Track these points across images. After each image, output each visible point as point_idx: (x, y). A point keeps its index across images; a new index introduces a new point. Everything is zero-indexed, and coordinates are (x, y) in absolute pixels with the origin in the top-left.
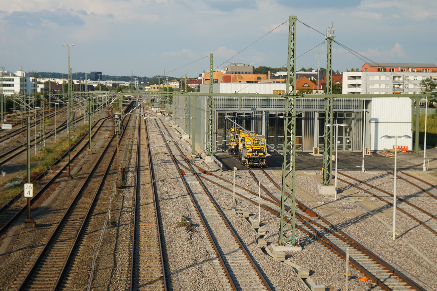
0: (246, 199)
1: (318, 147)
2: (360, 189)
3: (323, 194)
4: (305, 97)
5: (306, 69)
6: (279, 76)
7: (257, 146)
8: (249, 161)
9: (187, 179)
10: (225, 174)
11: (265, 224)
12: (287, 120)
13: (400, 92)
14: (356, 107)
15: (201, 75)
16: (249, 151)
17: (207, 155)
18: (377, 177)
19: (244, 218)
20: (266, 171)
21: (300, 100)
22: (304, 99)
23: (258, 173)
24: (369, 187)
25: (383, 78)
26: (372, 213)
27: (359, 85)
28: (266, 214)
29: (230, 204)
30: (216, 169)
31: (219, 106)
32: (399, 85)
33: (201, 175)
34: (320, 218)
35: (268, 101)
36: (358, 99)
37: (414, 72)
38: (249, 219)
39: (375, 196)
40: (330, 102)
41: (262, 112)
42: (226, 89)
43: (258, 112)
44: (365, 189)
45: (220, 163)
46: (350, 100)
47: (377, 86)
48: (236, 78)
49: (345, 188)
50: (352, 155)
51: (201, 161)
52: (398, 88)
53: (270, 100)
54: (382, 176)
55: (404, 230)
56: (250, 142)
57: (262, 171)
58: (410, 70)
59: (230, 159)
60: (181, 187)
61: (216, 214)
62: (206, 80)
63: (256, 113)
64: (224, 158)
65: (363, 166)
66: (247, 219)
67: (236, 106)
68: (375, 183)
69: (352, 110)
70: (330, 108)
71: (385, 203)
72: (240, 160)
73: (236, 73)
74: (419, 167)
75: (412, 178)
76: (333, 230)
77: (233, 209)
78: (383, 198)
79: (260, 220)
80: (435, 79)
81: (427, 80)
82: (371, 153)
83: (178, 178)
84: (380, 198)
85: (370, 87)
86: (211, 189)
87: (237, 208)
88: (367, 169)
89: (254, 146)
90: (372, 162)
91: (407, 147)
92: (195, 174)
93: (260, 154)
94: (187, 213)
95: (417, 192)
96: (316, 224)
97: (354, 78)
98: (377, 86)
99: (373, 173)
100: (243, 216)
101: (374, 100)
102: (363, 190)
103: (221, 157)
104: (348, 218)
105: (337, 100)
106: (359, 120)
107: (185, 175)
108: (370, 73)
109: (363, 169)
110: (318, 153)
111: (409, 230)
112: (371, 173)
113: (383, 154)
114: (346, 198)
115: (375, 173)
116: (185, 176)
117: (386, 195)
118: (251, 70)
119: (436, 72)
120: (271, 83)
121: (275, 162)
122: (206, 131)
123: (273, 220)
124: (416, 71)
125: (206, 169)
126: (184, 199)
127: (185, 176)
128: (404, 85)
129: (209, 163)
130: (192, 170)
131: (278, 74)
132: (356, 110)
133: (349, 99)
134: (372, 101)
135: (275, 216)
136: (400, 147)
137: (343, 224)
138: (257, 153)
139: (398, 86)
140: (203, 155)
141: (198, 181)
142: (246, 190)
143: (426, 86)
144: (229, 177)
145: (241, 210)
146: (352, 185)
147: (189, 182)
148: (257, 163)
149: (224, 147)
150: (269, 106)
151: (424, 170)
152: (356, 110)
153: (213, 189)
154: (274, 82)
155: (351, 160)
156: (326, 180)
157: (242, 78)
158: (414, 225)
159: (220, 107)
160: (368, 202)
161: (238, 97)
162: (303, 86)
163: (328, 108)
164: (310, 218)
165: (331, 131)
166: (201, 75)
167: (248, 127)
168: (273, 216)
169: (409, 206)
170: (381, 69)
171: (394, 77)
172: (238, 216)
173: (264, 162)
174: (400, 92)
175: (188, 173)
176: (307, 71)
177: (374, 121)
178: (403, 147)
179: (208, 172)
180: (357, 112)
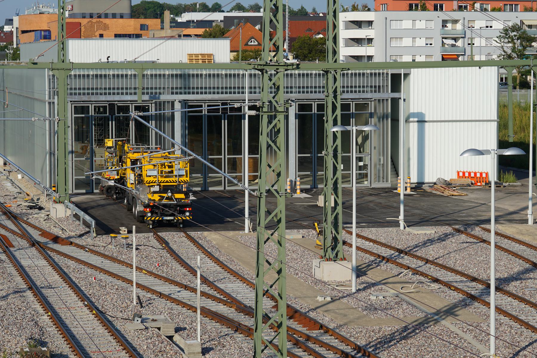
0: (161, 295)
1: (298, 179)
2: (402, 266)
3: (326, 279)
4: (304, 69)
5: (246, 5)
6: (188, 22)
7: (171, 179)
8: (152, 212)
9: (17, 254)
10: (102, 242)
11: (212, 349)
12: (265, 120)
13: (458, 56)
14: (378, 89)
15: (12, 20)
16: (152, 189)
17: (55, 202)
18: (431, 241)
19: (163, 337)
20: (192, 234)
21: (291, 75)
22: (301, 72)
23: (176, 239)
24: (421, 263)
25: (421, 25)
26: (436, 317)
27: (370, 41)
28: (209, 327)
29: (127, 307)
30: (78, 233)
31: (86, 91)
32: (455, 39)
33: (48, 245)
34: (327, 331)
35: (184, 78)
36: (381, 71)
37: (486, 10)
38: (175, 339)
39: (436, 280)
40: (335, 79)
41: (173, 103)
42: (83, 52)
43: (164, 102)
44: (413, 266)
45: (88, 218)
46: (364, 74)
47: (407, 42)
48: (92, 26)
49: (369, 266)
50: (371, 195)
51: (43, 214)
52: (453, 46)
53: (189, 75)
54: (442, 239)
55: (511, 351)
56: (160, 167)
57: (182, 234)
58: (477, 5)
59: (110, 209)
60: (10, 275)
61: (101, 330)
62: (24, 32)
63: (160, 105)
64: (93, 208)
65: (401, 217)
66: (171, 338)
67: (120, 90)
68: (431, 252)
69: (369, 95)
70: (335, 91)
71: (461, 296)
72: (130, 210)
73: (91, 16)
74: (516, 217)
75: (506, 240)
76: (359, 355)
77: (136, 318)
78: (455, 284)
79: (201, 339)
80: (530, 26)
81: (514, 28)
82: (412, 188)
83: (15, 251)
84: (448, 285)
85: (394, 43)
86: (78, 275)
87: (144, 316)
88: (409, 223)
89: (163, 179)
90: (417, 208)
91: (487, 174)
92: (34, 243)
93: (178, 196)
94: (36, 330)
95: (521, 269)
96: (323, 344)
97: (358, 24)
98: (407, 42)
99: (423, 232)
100: (161, 332)
101: (414, 72)
102: (409, 268)
103: (85, 206)
104: (388, 329)
105: (299, 75)
106: (384, 117)
107: (13, 247)
108: (391, 15)
109: (402, 223)
110: (298, 191)
111: (519, 351)
112: (419, 232)
113: (437, 190)
114: (376, 288)
115: (428, 232)
116: (12, 249)
117: (458, 278)
118: (126, 10)
119: (531, 10)
120: (172, 37)
121: (214, 211)
122: (48, 148)
123: (228, 338)
124: (489, 8)
125: (57, 232)
126: (22, 299)
127: (12, 249)
128: (466, 39)
129: (60, 220)
130: (25, 235)
131: (185, 17)
132: (377, 96)
133: (361, 72)
134: (411, 76)
135: (230, 331)
136: (472, 175)
137: (380, 343)
138: (170, 194)
139: (453, 42)
140: (43, 202)
141: (46, 259)
142: (157, 276)
143: (513, 40)
144: (112, 250)
145: (153, 320)
146: (384, 258)
147: (24, 263)
148: (170, 216)
149: (86, 184)
150: (186, 89)
151: (530, 222)
152: (377, 96)
153: (82, 276)
154: (180, 36)
155: (371, 205)
156: (330, 250)
157: (106, 27)
158: (529, 340)
159: (80, 94)
160: (424, 295)
161: (103, 72)
162: (247, 44)
163: (331, 91)
164: (307, 332)
165: (339, 142)
166: (10, 22)
167: (142, 136)
168: (225, 330)
169: (510, 299)
170: (417, 6)
171: (444, 23)
172: (150, 334)
173: (188, 214)
174: (458, 56)
175: (18, 242)
176: (248, 11)
177: (416, 119)
178: (478, 175)
179: (63, 239)
180: (379, 100)
